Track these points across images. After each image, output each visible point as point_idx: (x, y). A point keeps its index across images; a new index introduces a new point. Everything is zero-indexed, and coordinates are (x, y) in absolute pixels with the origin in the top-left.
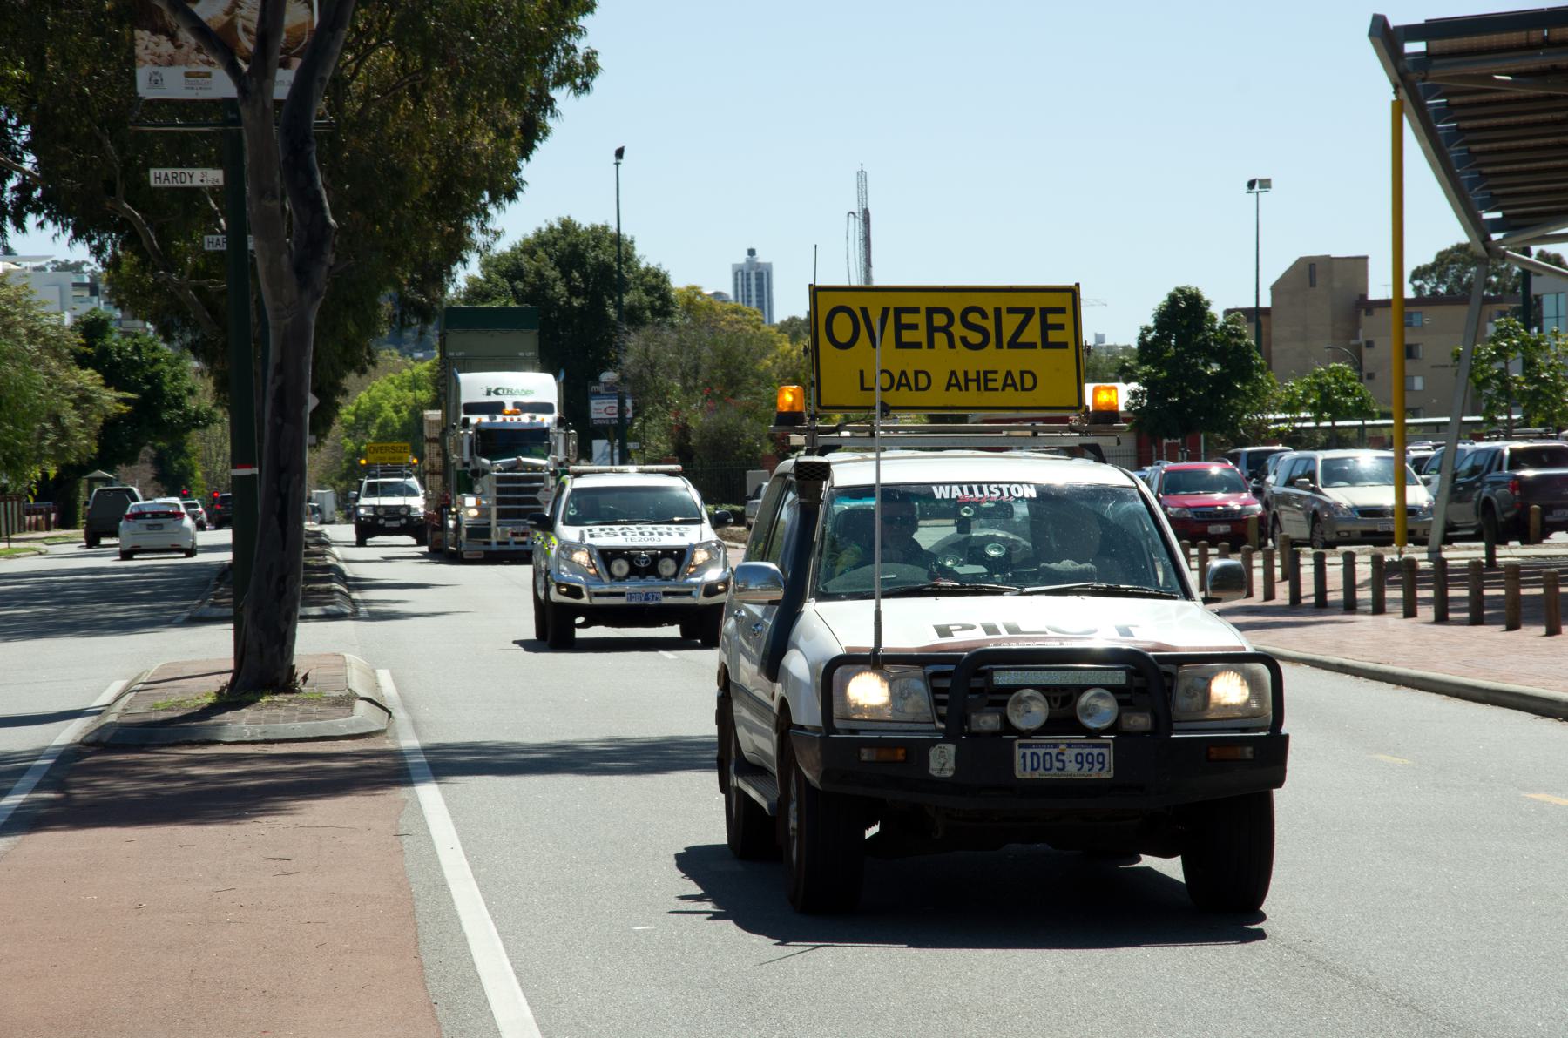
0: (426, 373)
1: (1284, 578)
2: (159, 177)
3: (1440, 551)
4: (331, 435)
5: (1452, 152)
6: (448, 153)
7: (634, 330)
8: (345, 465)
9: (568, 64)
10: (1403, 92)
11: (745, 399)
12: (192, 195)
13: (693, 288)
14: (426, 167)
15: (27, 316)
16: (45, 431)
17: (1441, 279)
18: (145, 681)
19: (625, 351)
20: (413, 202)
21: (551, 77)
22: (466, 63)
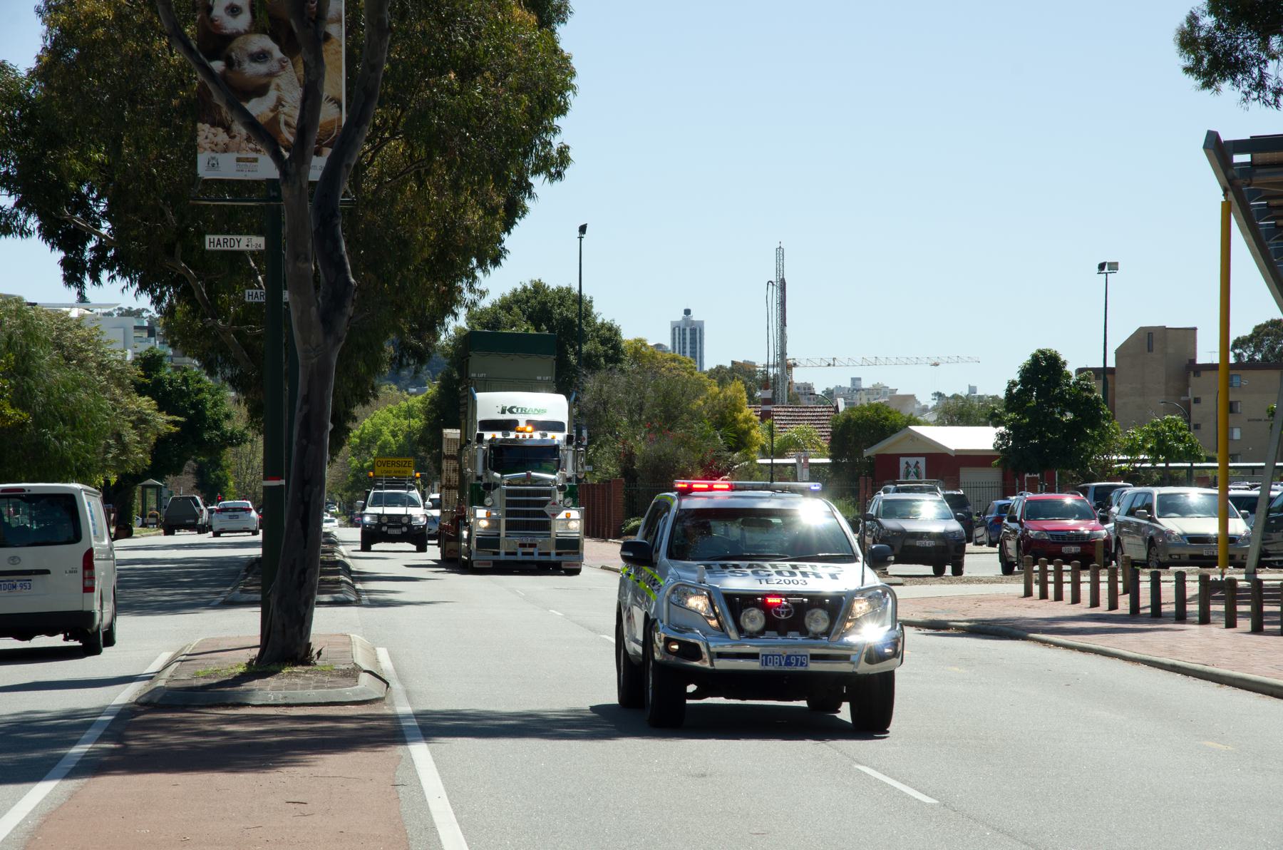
0: (419, 405)
1: (1125, 592)
2: (212, 242)
3: (1255, 573)
4: (341, 454)
5: (1270, 245)
6: (445, 227)
7: (591, 374)
8: (351, 479)
9: (545, 156)
10: (1231, 194)
11: (680, 432)
12: (237, 257)
13: (640, 340)
14: (427, 237)
15: (97, 352)
16: (109, 446)
17: (1258, 348)
18: (188, 652)
19: (583, 390)
20: (415, 266)
21: (530, 167)
22: (461, 153)
